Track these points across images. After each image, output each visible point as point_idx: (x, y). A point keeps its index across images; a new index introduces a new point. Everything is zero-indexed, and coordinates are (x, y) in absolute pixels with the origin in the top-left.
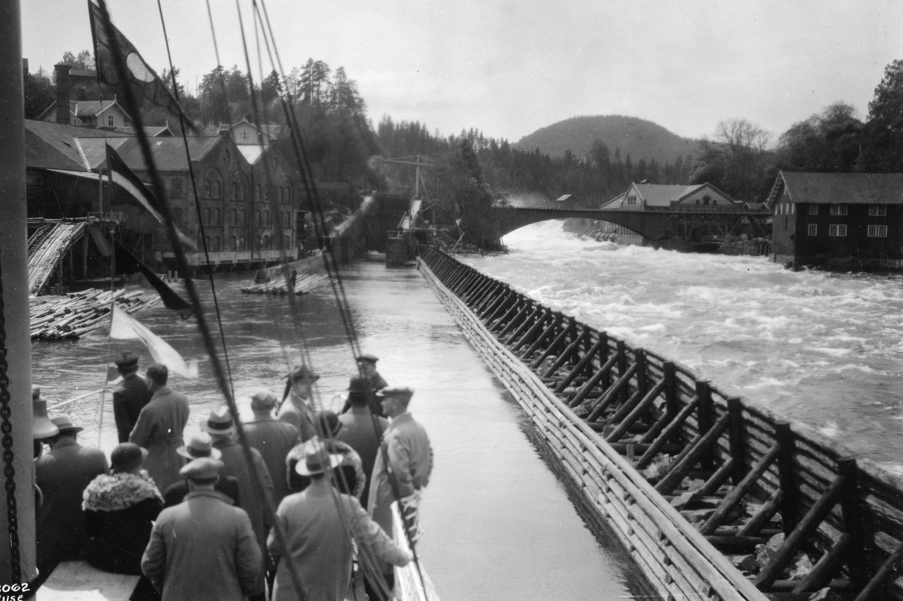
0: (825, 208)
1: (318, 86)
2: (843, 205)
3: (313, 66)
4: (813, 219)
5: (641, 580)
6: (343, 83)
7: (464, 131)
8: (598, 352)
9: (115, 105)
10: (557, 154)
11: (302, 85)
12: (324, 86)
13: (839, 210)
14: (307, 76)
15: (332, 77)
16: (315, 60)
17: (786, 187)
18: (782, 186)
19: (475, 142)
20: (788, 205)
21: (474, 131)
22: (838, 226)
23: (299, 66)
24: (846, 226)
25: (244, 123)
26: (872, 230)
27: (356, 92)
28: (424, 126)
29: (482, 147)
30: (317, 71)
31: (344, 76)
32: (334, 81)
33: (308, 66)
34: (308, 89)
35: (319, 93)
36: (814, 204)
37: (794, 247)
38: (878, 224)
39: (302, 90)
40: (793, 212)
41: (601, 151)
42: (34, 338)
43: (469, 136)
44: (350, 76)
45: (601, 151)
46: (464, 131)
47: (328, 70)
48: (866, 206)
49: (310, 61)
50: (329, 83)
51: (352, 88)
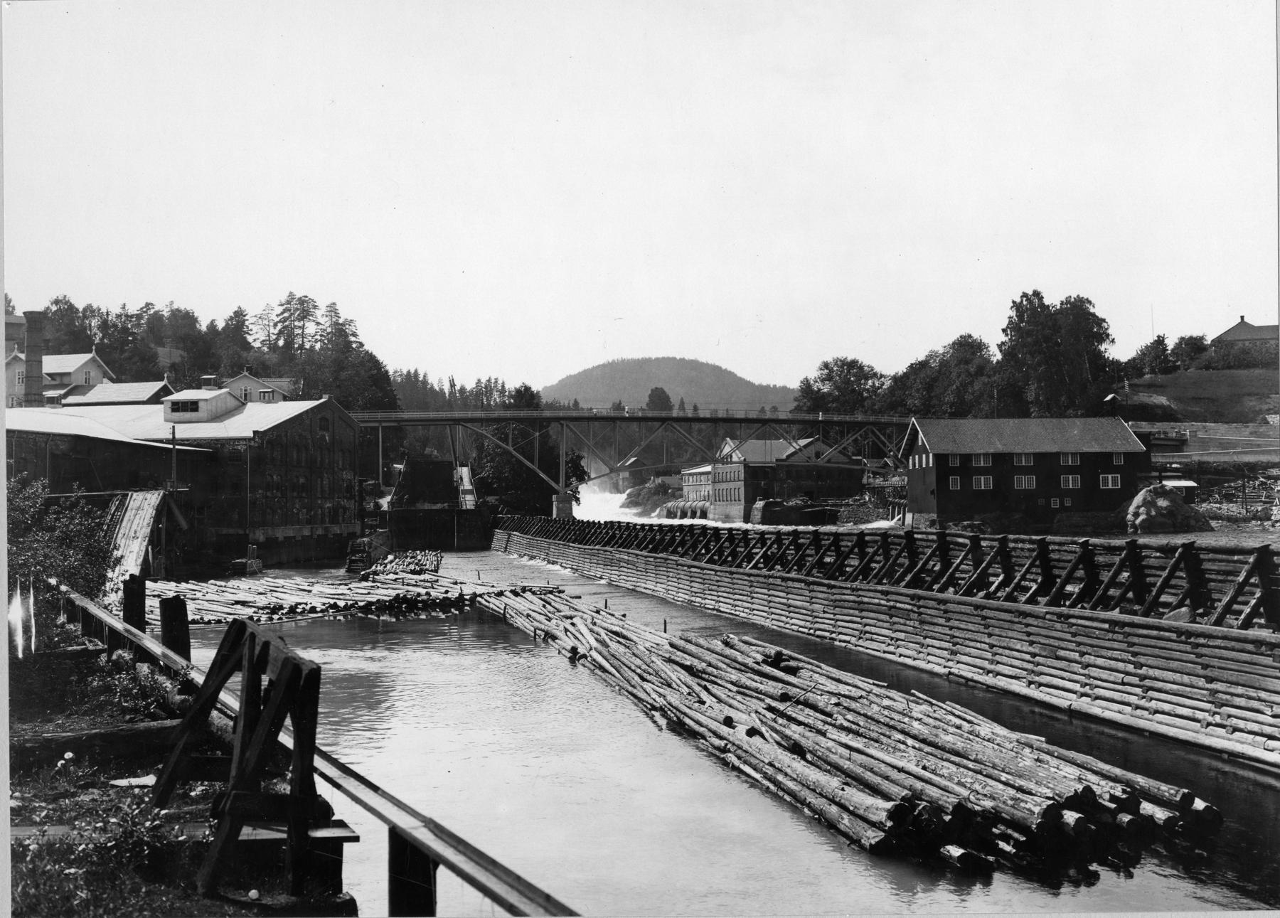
0: (966, 458)
1: (303, 327)
2: (986, 455)
3: (294, 301)
4: (954, 471)
5: (437, 832)
6: (337, 324)
7: (479, 381)
8: (1182, 565)
9: (93, 360)
10: (601, 407)
11: (280, 326)
12: (311, 328)
13: (1023, 459)
14: (286, 315)
15: (320, 314)
16: (298, 295)
17: (921, 434)
18: (915, 433)
19: (496, 395)
20: (924, 456)
21: (493, 381)
22: (1070, 477)
23: (275, 304)
24: (1119, 476)
25: (245, 375)
26: (1020, 481)
27: (354, 335)
28: (425, 376)
29: (504, 401)
30: (302, 308)
31: (337, 316)
32: (326, 322)
33: (289, 302)
34: (287, 333)
35: (303, 336)
36: (1119, 454)
37: (148, 530)
38: (1025, 474)
39: (280, 332)
40: (931, 465)
41: (659, 398)
42: (1043, 545)
43: (486, 387)
44: (344, 315)
45: (659, 398)
46: (479, 381)
47: (315, 307)
48: (1057, 455)
49: (291, 295)
50: (318, 324)
51: (349, 329)
